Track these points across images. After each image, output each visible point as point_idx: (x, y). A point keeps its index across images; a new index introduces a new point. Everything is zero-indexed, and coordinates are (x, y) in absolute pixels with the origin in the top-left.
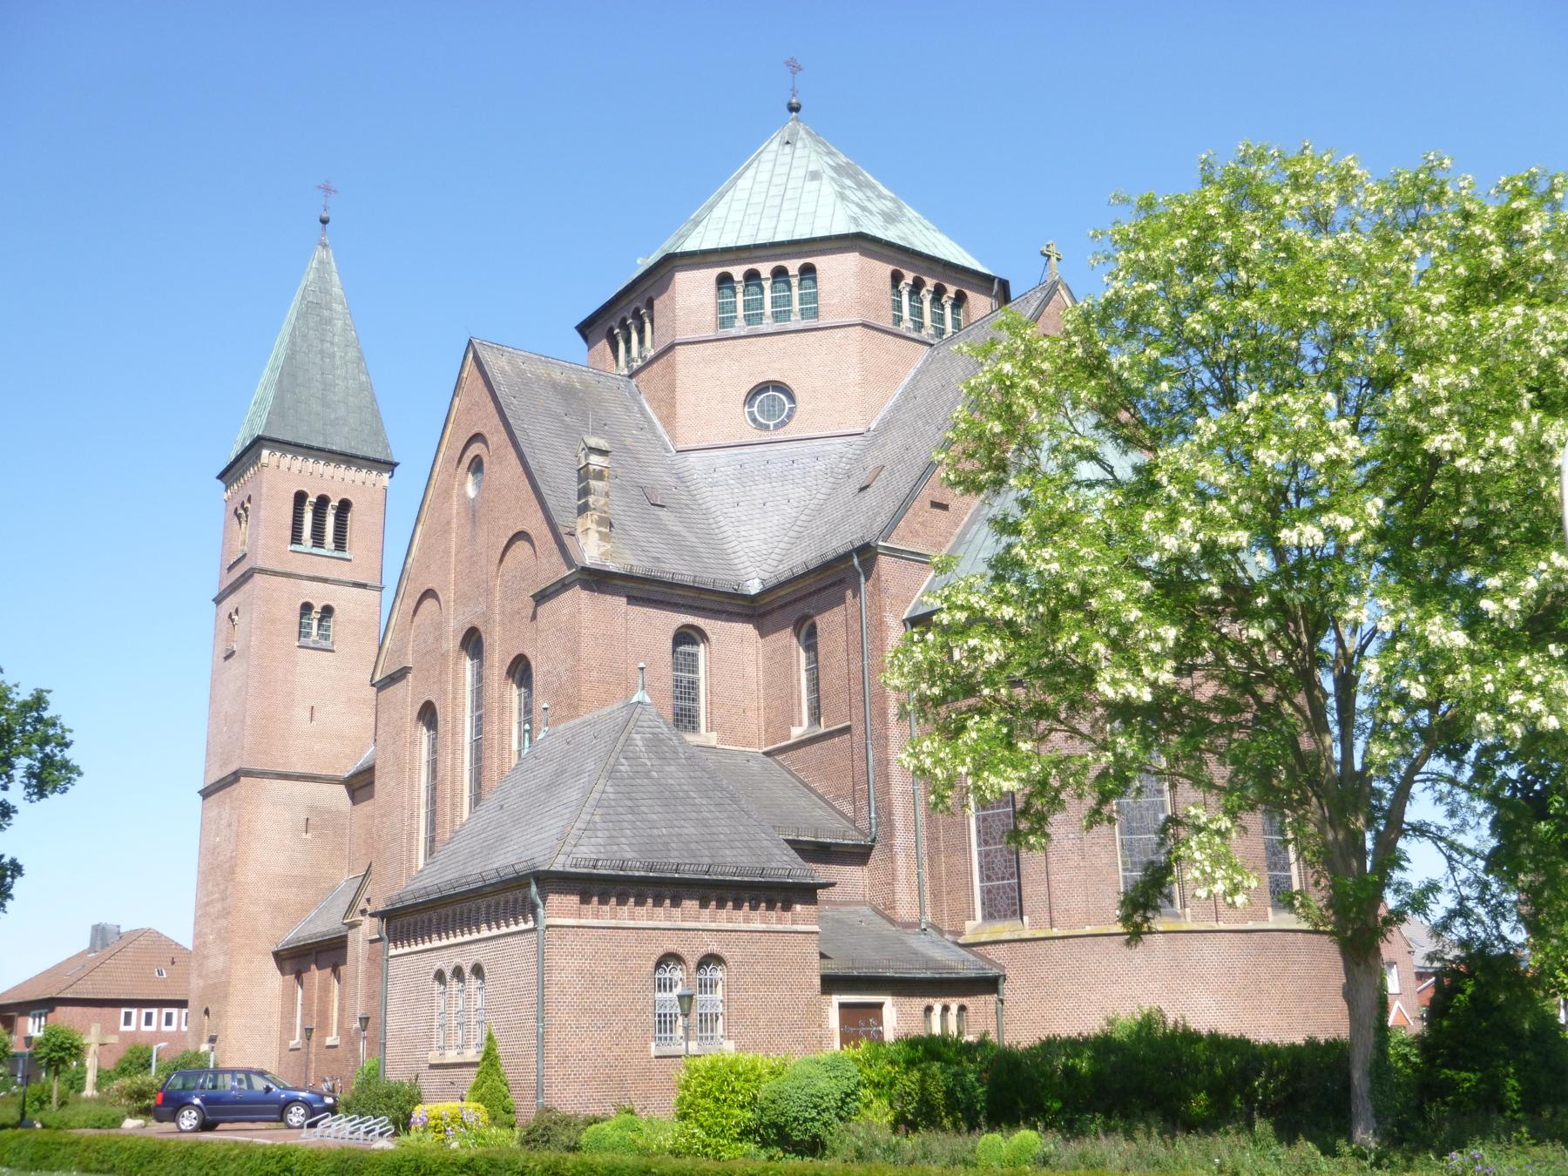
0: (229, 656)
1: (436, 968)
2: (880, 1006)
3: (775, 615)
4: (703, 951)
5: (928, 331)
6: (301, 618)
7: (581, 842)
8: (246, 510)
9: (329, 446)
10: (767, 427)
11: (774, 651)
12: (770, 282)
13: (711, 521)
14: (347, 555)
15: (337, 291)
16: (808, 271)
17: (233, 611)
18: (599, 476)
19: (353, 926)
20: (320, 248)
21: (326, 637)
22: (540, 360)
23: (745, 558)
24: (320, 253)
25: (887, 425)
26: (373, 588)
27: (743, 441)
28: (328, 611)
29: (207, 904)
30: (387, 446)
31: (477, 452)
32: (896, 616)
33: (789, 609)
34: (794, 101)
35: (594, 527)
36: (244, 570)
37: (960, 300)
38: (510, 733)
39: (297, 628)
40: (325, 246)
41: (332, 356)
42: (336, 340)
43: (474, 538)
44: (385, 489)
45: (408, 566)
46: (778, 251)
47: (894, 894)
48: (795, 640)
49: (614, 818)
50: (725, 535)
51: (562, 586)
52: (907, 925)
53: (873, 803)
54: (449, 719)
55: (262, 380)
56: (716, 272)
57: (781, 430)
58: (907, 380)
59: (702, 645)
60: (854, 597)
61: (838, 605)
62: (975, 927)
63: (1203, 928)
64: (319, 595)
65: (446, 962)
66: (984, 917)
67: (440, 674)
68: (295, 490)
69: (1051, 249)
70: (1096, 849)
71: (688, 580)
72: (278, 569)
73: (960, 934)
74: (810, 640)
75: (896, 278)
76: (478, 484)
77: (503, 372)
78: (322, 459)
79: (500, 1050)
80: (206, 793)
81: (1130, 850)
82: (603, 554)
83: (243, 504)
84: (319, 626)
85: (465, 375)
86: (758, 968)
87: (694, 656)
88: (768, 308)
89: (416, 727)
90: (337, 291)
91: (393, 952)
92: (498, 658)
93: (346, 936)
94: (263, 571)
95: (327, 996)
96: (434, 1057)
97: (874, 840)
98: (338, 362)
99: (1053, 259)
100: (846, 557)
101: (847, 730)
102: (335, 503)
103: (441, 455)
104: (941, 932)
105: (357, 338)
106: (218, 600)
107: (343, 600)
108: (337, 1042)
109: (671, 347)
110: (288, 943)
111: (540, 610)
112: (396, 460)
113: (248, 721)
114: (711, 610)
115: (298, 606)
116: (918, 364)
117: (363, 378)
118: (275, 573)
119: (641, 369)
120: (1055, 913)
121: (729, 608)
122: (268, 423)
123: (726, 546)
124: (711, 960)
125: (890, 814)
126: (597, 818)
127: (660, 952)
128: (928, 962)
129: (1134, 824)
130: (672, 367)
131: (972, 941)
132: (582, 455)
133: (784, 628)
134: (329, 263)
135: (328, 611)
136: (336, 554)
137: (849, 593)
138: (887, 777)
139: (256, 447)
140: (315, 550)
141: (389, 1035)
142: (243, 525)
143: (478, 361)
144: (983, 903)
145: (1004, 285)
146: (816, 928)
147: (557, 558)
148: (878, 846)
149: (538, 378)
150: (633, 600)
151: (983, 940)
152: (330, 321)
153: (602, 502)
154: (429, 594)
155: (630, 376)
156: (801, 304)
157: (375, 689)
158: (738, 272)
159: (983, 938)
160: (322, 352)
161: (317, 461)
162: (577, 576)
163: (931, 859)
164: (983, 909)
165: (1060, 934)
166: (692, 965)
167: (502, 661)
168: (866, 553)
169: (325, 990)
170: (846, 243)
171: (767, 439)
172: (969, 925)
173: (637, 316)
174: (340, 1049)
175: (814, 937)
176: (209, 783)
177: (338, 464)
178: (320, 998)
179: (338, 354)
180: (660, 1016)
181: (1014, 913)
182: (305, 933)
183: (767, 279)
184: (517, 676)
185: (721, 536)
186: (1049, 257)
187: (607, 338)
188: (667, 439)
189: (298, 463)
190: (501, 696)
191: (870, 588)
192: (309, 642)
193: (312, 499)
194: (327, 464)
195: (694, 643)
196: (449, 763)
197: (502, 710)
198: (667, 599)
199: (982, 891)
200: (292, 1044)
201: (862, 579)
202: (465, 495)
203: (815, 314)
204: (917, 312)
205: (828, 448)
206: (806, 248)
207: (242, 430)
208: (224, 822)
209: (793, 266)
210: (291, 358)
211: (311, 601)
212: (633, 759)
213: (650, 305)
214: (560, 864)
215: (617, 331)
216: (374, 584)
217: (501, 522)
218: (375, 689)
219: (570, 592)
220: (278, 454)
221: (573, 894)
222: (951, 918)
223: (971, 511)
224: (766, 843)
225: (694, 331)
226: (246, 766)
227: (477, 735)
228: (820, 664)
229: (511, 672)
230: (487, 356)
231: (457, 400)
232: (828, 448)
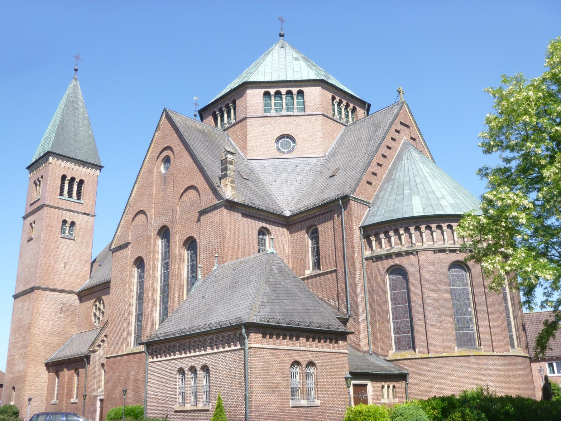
0: (30, 240)
1: (178, 367)
2: (366, 385)
3: (297, 225)
4: (308, 360)
5: (344, 120)
6: (62, 226)
7: (261, 310)
8: (39, 181)
9: (76, 158)
10: (284, 152)
11: (296, 239)
12: (285, 96)
13: (266, 187)
14: (81, 202)
15: (81, 97)
16: (300, 93)
17: (32, 222)
18: (231, 163)
19: (94, 351)
20: (74, 80)
21: (71, 234)
22: (191, 120)
23: (281, 202)
24: (74, 82)
25: (333, 154)
26: (92, 216)
27: (275, 157)
28: (73, 224)
29: (15, 342)
30: (99, 160)
31: (167, 154)
32: (357, 225)
33: (304, 223)
34: (282, 33)
35: (229, 183)
36: (40, 204)
37: (354, 110)
38: (184, 270)
39: (60, 230)
40: (76, 80)
41: (78, 123)
42: (80, 116)
43: (165, 189)
44: (98, 176)
45: (130, 201)
46: (288, 84)
47: (360, 339)
48: (306, 235)
49: (272, 301)
50: (272, 193)
51: (215, 207)
52: (365, 352)
53: (349, 301)
54: (151, 264)
55: (47, 130)
56: (263, 90)
57: (290, 154)
58: (338, 137)
59: (268, 236)
60: (338, 217)
61: (329, 220)
62: (392, 353)
63: (489, 354)
64: (70, 217)
65: (186, 365)
66: (396, 349)
67: (147, 245)
68: (62, 174)
69: (401, 89)
70: (446, 321)
71: (264, 208)
72: (54, 205)
73: (387, 356)
74: (315, 235)
75: (333, 98)
76: (167, 168)
77: (179, 122)
78: (74, 163)
79: (224, 404)
80: (16, 297)
81: (458, 322)
82: (232, 195)
83: (38, 179)
84: (69, 229)
85: (161, 123)
86: (328, 368)
87: (264, 240)
88: (284, 106)
89: (132, 267)
90: (81, 97)
91: (151, 360)
92: (177, 239)
93: (90, 355)
94: (48, 206)
95: (72, 382)
96: (177, 407)
97: (349, 317)
98: (80, 125)
99: (401, 93)
100: (336, 200)
101: (335, 271)
102: (78, 180)
103: (148, 156)
104: (378, 355)
105: (88, 117)
106: (25, 218)
107: (79, 219)
108: (77, 401)
109: (245, 119)
110: (52, 359)
111: (202, 218)
112: (103, 165)
113: (39, 267)
114: (272, 221)
115: (61, 221)
116: (341, 132)
117: (90, 132)
118: (52, 207)
119: (234, 125)
120: (430, 348)
121: (278, 221)
122: (52, 146)
123: (273, 197)
124: (311, 364)
125: (357, 305)
126: (265, 301)
127: (292, 360)
128: (382, 368)
129: (459, 312)
130: (245, 126)
131: (393, 359)
132: (223, 154)
133: (302, 230)
134: (78, 86)
135: (73, 224)
136: (77, 201)
137: (335, 216)
138: (356, 290)
139: (48, 155)
140: (69, 199)
141: (149, 397)
142: (38, 187)
143: (169, 118)
144: (396, 343)
145: (369, 105)
146: (346, 351)
147: (211, 195)
148: (351, 319)
149: (192, 127)
150: (244, 215)
151: (398, 358)
152: (77, 109)
153: (232, 174)
154: (142, 212)
155: (224, 130)
156: (297, 105)
157: (111, 252)
158: (272, 91)
159: (398, 358)
160: (74, 120)
161: (71, 163)
162: (223, 203)
163: (372, 325)
164: (396, 346)
165: (433, 356)
166: (304, 366)
167: (180, 239)
168: (346, 199)
169: (71, 379)
170: (316, 83)
171: (285, 157)
172: (391, 352)
173: (228, 107)
174: (78, 404)
175: (346, 355)
176: (17, 292)
177: (79, 165)
178: (68, 382)
179: (80, 122)
180: (292, 388)
181: (410, 347)
182: (60, 356)
183: (284, 95)
184: (187, 246)
185: (270, 193)
186: (400, 92)
187: (212, 115)
188: (242, 155)
189: (64, 163)
190: (180, 254)
191: (346, 214)
192: (65, 236)
193: (69, 178)
194: (75, 164)
195: (264, 235)
196: (151, 282)
197: (180, 260)
198: (256, 216)
199: (395, 338)
200: (53, 402)
201: (343, 210)
202: (160, 172)
203: (304, 110)
204: (340, 113)
205: (310, 162)
206: (300, 84)
207: (38, 150)
208: (25, 308)
209: (295, 90)
210: (62, 122)
211: (66, 219)
212: (274, 276)
213: (234, 103)
214: (254, 319)
215: (217, 113)
216: (92, 214)
217: (181, 182)
218: (111, 252)
219: (219, 210)
220: (56, 159)
221: (259, 333)
222: (382, 349)
223: (379, 186)
224: (327, 314)
225: (255, 113)
226: (37, 285)
227: (165, 270)
228: (320, 244)
229: (185, 244)
230: (172, 116)
231: (157, 133)
232: (310, 162)
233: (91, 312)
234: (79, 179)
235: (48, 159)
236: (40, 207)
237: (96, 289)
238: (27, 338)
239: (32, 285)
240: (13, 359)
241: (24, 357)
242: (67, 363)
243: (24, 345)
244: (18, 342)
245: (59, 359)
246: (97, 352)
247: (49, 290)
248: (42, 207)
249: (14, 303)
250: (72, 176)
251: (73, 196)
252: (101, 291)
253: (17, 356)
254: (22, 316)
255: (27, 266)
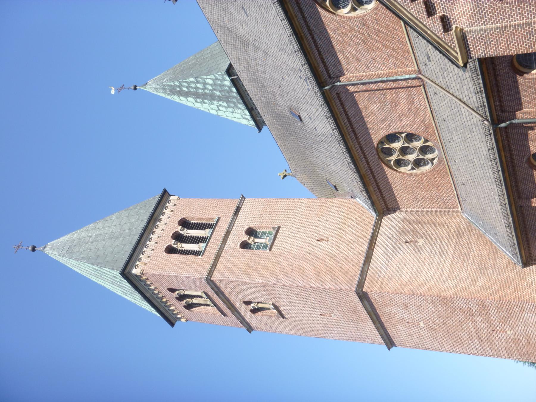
19: (463, 39)
42: (90, 235)
68: (164, 253)
72: (211, 263)
115: (242, 251)
133: (516, 82)
210: (88, 260)
233: (410, 174)
234: (178, 226)
235: (136, 276)
236: (217, 290)
237: (363, 165)
238: (465, 307)
239: (356, 300)
240: (515, 343)
241: (507, 311)
242: (519, 198)
243: (480, 314)
244: (477, 332)
245: (510, 226)
246: (465, 29)
247: (367, 266)
248: (211, 284)
249: (402, 346)
250: (170, 237)
251: (204, 236)
252: (364, 148)
253: (509, 333)
254: (422, 324)
255: (325, 315)
